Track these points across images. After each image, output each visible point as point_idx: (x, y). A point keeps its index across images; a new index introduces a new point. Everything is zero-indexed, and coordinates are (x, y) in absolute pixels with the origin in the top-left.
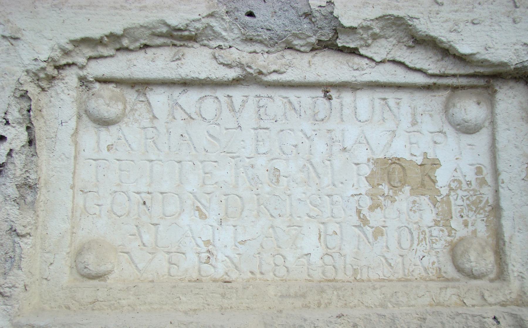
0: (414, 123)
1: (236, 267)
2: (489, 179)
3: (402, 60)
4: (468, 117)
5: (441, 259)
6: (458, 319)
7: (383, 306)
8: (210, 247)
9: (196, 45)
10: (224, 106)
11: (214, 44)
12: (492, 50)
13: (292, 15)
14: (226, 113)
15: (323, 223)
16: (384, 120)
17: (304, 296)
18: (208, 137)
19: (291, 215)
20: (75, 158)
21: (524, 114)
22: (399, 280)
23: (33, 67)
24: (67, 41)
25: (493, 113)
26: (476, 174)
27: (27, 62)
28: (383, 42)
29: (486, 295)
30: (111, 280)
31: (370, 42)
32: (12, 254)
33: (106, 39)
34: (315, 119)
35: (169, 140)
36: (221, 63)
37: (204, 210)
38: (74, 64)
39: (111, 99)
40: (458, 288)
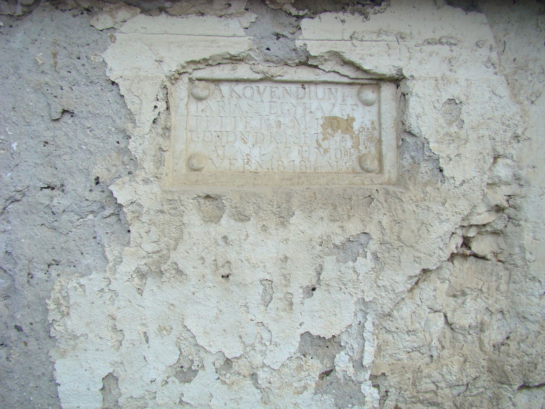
0: (344, 100)
1: (261, 166)
2: (377, 127)
3: (338, 71)
4: (368, 98)
5: (355, 163)
6: (361, 190)
7: (327, 184)
8: (249, 157)
9: (243, 63)
10: (256, 92)
11: (251, 62)
12: (379, 68)
13: (287, 49)
14: (256, 95)
15: (301, 146)
16: (330, 98)
17: (291, 179)
18: (248, 106)
19: (286, 142)
20: (187, 115)
21: (393, 98)
22: (335, 173)
23: (169, 74)
24: (184, 62)
25: (379, 97)
26: (371, 125)
27: (167, 72)
28: (329, 62)
29: (374, 180)
30: (204, 172)
31: (323, 62)
32: (160, 159)
33: (202, 61)
34: (298, 98)
35: (230, 107)
36: (254, 72)
37: (246, 140)
38: (187, 72)
39: (203, 88)
40: (361, 177)
